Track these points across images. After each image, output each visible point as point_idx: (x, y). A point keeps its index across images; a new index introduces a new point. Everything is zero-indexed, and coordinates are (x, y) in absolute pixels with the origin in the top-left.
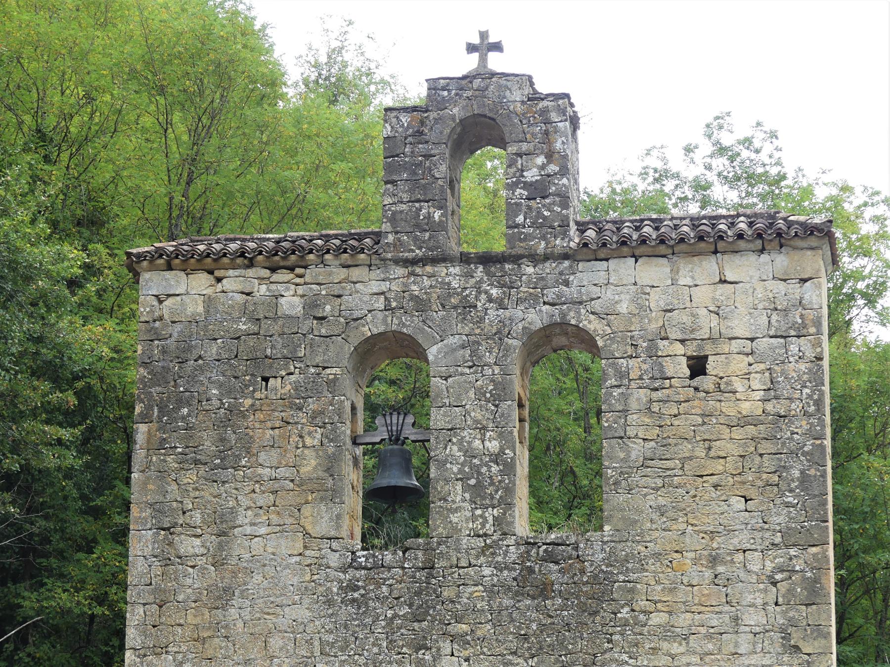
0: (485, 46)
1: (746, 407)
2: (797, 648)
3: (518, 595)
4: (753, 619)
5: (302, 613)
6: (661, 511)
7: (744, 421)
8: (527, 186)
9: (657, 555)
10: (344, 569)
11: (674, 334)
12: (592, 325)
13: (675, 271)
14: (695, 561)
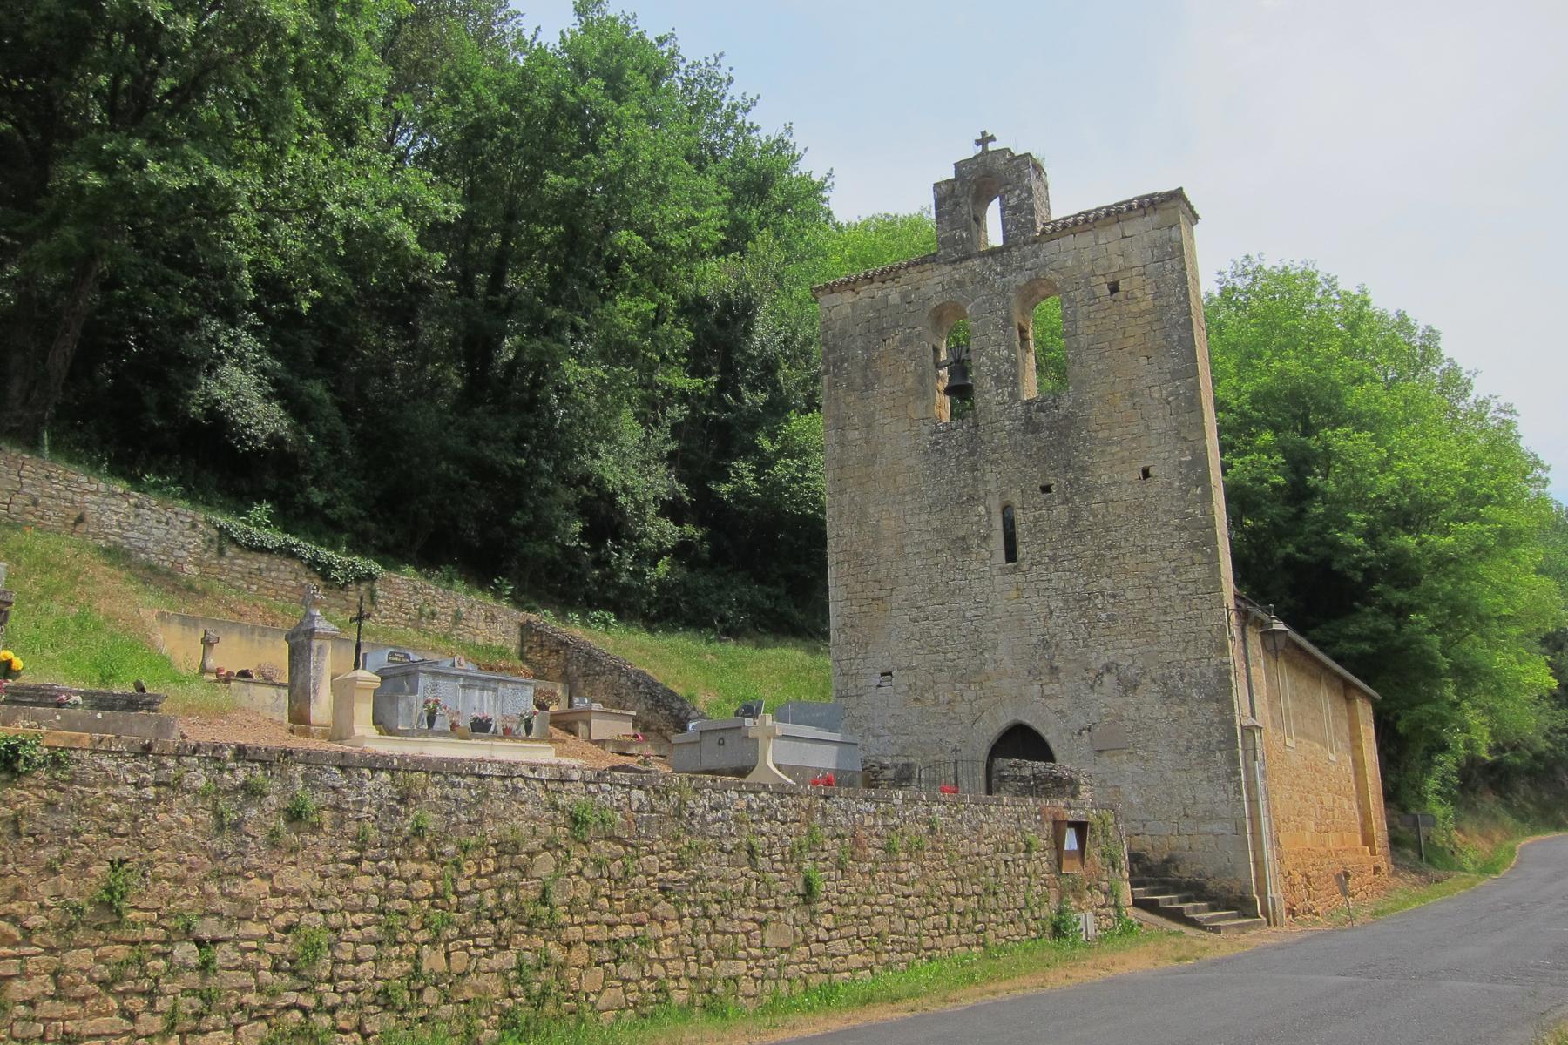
0: (985, 140)
1: (1143, 305)
2: (1185, 439)
3: (1026, 431)
4: (1157, 426)
5: (913, 462)
6: (1100, 372)
7: (1142, 313)
8: (1011, 208)
9: (1100, 398)
10: (932, 434)
11: (1100, 272)
12: (1053, 276)
13: (1097, 237)
14: (1122, 398)
